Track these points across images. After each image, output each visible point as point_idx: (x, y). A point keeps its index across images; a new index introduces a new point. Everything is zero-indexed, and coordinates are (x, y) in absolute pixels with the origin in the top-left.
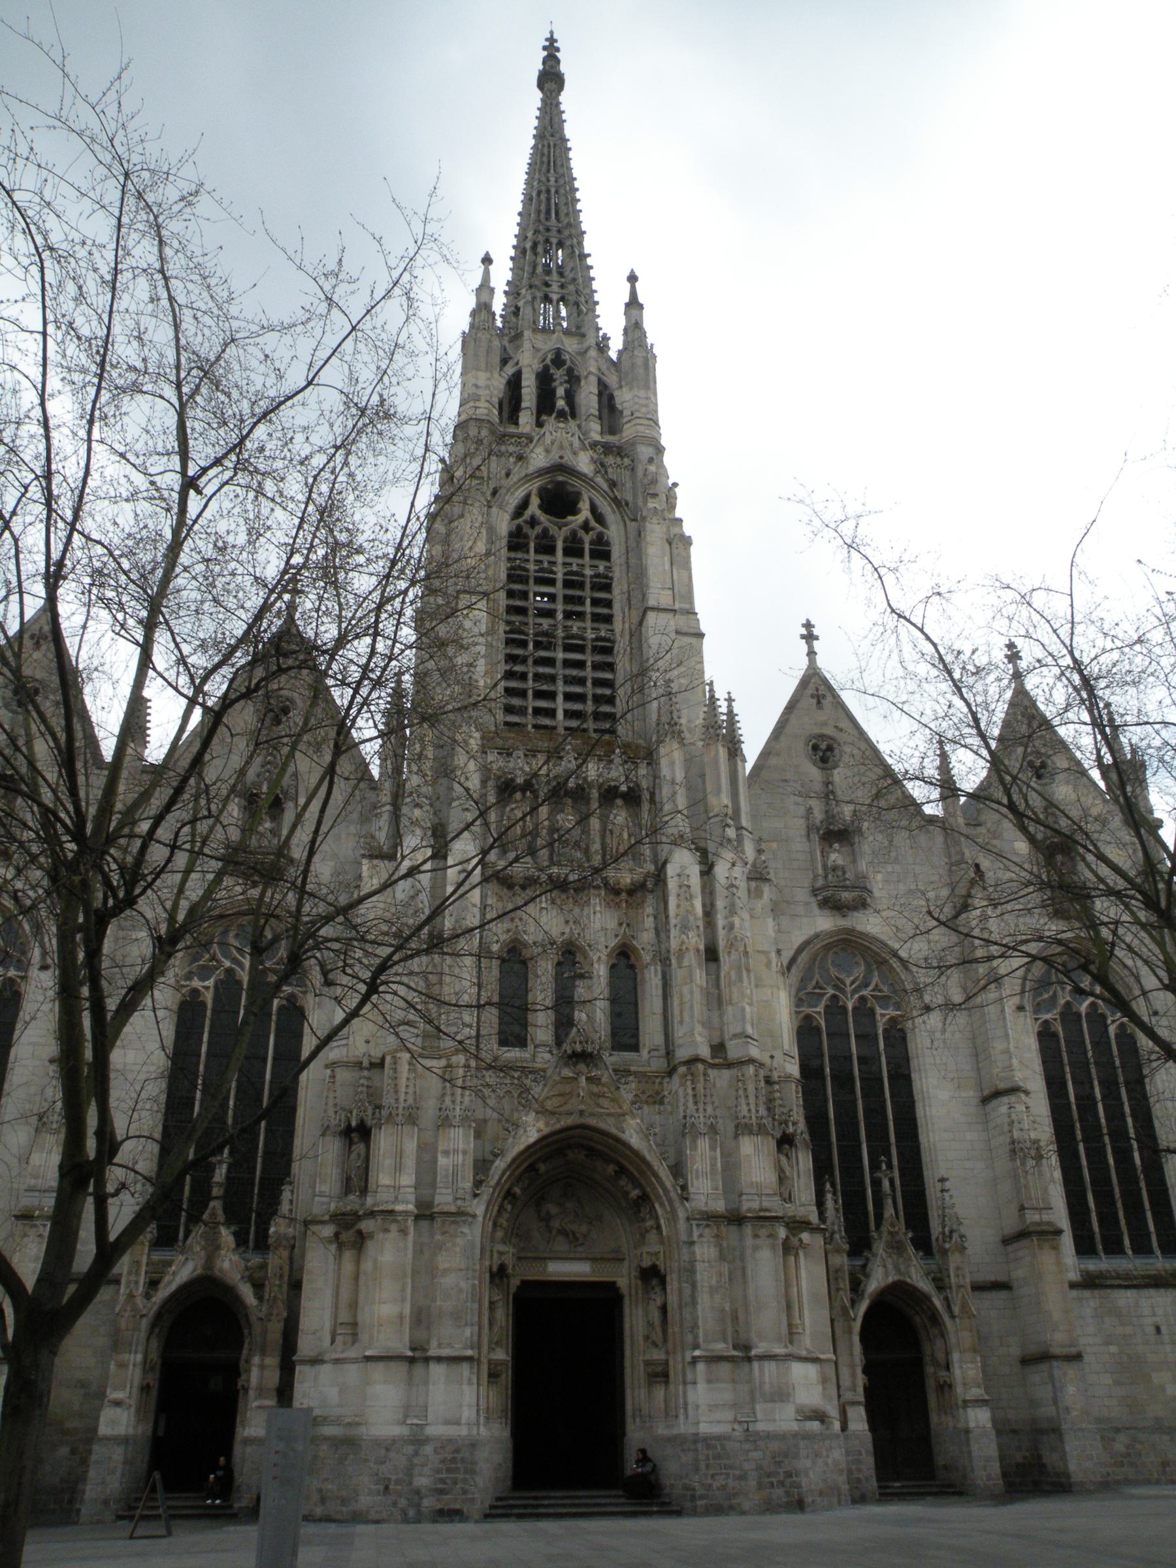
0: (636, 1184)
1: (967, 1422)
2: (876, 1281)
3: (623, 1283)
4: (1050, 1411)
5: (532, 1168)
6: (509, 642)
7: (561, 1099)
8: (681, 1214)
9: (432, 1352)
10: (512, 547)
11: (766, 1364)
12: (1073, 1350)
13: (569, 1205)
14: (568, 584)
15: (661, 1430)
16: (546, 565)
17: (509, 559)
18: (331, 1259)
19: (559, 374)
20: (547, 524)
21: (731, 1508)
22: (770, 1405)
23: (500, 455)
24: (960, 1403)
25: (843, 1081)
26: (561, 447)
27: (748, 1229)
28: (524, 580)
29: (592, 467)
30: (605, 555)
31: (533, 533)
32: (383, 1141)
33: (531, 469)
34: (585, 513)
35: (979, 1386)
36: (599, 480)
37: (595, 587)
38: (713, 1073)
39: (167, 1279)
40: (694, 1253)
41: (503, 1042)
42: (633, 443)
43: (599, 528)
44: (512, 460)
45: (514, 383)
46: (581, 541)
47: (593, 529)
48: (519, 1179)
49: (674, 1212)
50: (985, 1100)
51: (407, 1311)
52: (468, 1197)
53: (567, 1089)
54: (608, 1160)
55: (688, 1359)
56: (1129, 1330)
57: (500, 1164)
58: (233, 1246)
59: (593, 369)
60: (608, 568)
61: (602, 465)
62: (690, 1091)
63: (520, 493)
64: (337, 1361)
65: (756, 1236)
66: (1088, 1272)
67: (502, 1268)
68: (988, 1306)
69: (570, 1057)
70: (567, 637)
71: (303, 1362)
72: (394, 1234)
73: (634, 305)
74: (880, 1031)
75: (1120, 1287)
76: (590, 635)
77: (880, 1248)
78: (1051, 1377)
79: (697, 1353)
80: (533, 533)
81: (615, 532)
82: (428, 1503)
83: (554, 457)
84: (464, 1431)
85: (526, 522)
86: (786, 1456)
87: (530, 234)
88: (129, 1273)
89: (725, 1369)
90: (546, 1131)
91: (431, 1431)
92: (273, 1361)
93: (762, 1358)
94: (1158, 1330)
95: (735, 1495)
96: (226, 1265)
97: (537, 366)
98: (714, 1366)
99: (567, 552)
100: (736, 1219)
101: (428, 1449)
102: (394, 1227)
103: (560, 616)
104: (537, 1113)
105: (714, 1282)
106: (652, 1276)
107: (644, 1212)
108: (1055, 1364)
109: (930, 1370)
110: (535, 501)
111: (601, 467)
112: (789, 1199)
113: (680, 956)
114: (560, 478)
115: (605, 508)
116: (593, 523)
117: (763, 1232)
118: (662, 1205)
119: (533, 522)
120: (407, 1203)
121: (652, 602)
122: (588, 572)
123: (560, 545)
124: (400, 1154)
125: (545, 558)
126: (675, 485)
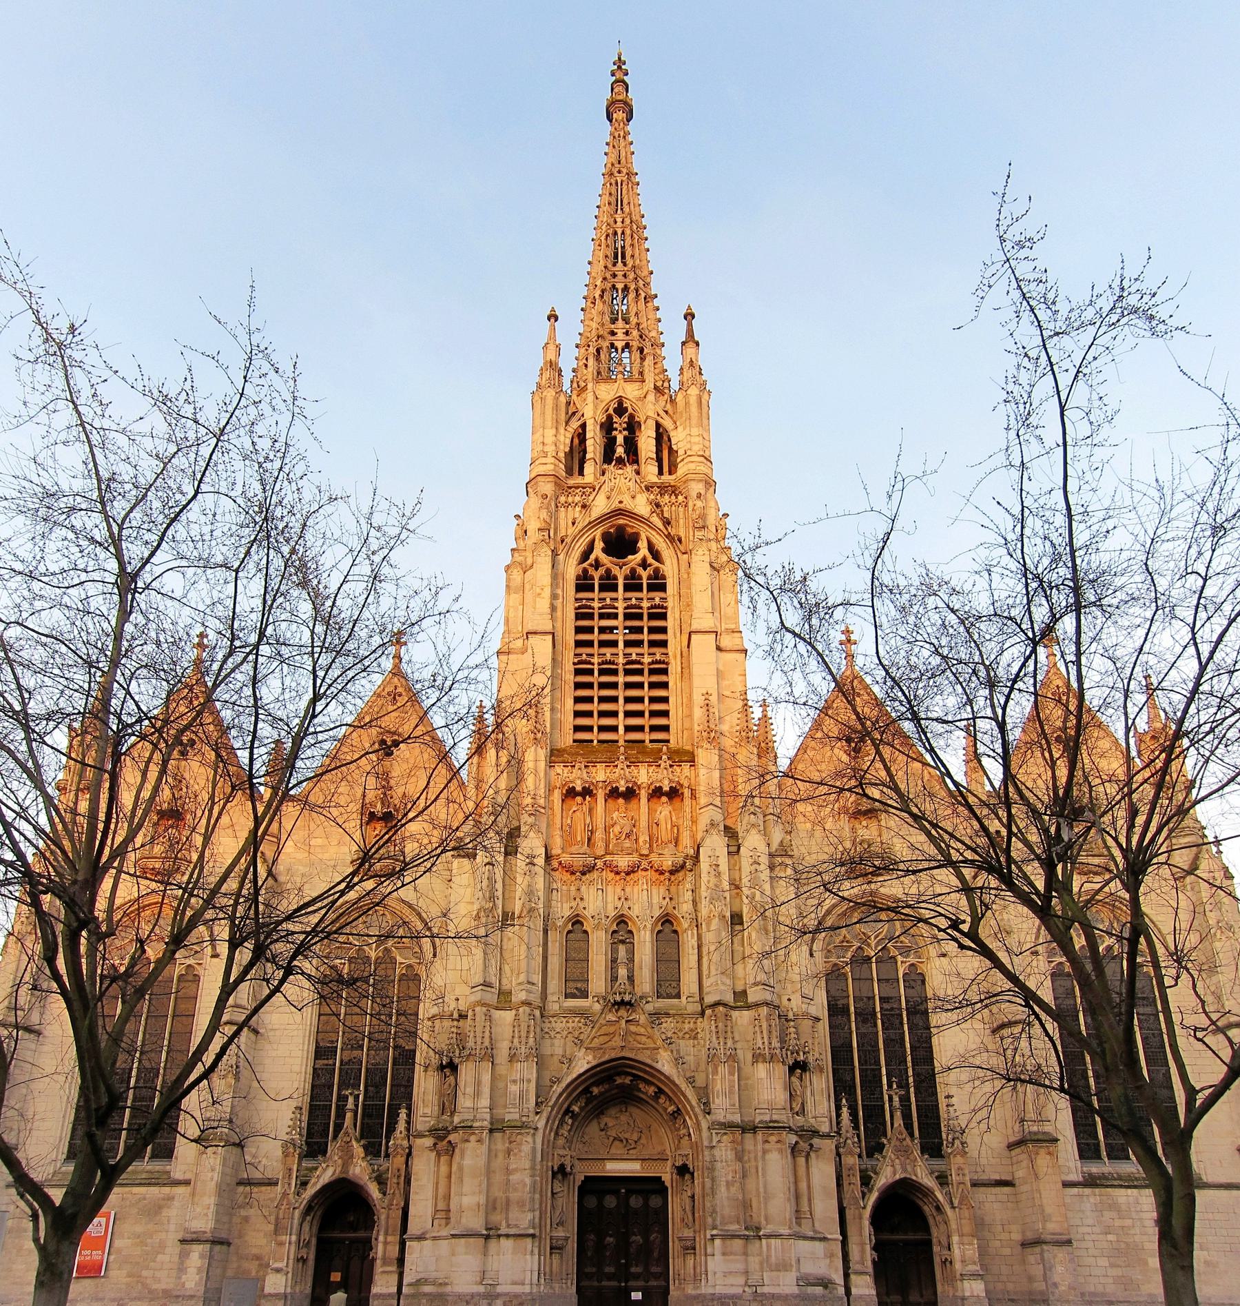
1: (963, 1290)
2: (885, 1177)
3: (666, 1178)
4: (1041, 1286)
5: (587, 1090)
6: (578, 672)
8: (704, 1125)
9: (503, 1231)
10: (579, 588)
12: (1065, 1237)
14: (628, 617)
15: (690, 1290)
16: (608, 601)
20: (609, 565)
22: (775, 1273)
23: (567, 505)
24: (958, 1276)
25: (866, 1016)
26: (620, 492)
27: (760, 1136)
29: (649, 508)
30: (662, 588)
31: (597, 575)
32: (466, 1072)
34: (643, 551)
35: (974, 1263)
38: (735, 1014)
39: (313, 1180)
43: (656, 564)
46: (640, 578)
48: (576, 1099)
49: (698, 1124)
50: (994, 1031)
53: (612, 1029)
55: (708, 1237)
56: (1128, 1222)
57: (558, 1089)
58: (363, 1155)
61: (658, 505)
62: (713, 1028)
64: (435, 1238)
65: (767, 1141)
66: (1090, 1174)
67: (562, 1167)
68: (992, 1202)
69: (613, 1005)
70: (628, 663)
71: (411, 1239)
73: (690, 339)
74: (901, 975)
75: (1121, 1186)
76: (647, 659)
77: (889, 1152)
78: (1043, 1259)
79: (715, 1232)
80: (597, 575)
81: (669, 568)
83: (615, 505)
84: (527, 1289)
85: (591, 565)
87: (598, 283)
89: (738, 1244)
90: (594, 1063)
92: (394, 1239)
93: (769, 1236)
96: (357, 1170)
97: (602, 418)
98: (728, 1242)
99: (627, 588)
100: (748, 1128)
102: (473, 1138)
104: (587, 1049)
105: (730, 1178)
107: (679, 1121)
108: (1045, 1247)
109: (936, 1249)
110: (599, 545)
112: (802, 1111)
114: (621, 522)
115: (661, 544)
116: (650, 560)
117: (773, 1139)
119: (597, 564)
121: (695, 627)
122: (645, 604)
123: (621, 582)
124: (478, 1083)
125: (608, 595)
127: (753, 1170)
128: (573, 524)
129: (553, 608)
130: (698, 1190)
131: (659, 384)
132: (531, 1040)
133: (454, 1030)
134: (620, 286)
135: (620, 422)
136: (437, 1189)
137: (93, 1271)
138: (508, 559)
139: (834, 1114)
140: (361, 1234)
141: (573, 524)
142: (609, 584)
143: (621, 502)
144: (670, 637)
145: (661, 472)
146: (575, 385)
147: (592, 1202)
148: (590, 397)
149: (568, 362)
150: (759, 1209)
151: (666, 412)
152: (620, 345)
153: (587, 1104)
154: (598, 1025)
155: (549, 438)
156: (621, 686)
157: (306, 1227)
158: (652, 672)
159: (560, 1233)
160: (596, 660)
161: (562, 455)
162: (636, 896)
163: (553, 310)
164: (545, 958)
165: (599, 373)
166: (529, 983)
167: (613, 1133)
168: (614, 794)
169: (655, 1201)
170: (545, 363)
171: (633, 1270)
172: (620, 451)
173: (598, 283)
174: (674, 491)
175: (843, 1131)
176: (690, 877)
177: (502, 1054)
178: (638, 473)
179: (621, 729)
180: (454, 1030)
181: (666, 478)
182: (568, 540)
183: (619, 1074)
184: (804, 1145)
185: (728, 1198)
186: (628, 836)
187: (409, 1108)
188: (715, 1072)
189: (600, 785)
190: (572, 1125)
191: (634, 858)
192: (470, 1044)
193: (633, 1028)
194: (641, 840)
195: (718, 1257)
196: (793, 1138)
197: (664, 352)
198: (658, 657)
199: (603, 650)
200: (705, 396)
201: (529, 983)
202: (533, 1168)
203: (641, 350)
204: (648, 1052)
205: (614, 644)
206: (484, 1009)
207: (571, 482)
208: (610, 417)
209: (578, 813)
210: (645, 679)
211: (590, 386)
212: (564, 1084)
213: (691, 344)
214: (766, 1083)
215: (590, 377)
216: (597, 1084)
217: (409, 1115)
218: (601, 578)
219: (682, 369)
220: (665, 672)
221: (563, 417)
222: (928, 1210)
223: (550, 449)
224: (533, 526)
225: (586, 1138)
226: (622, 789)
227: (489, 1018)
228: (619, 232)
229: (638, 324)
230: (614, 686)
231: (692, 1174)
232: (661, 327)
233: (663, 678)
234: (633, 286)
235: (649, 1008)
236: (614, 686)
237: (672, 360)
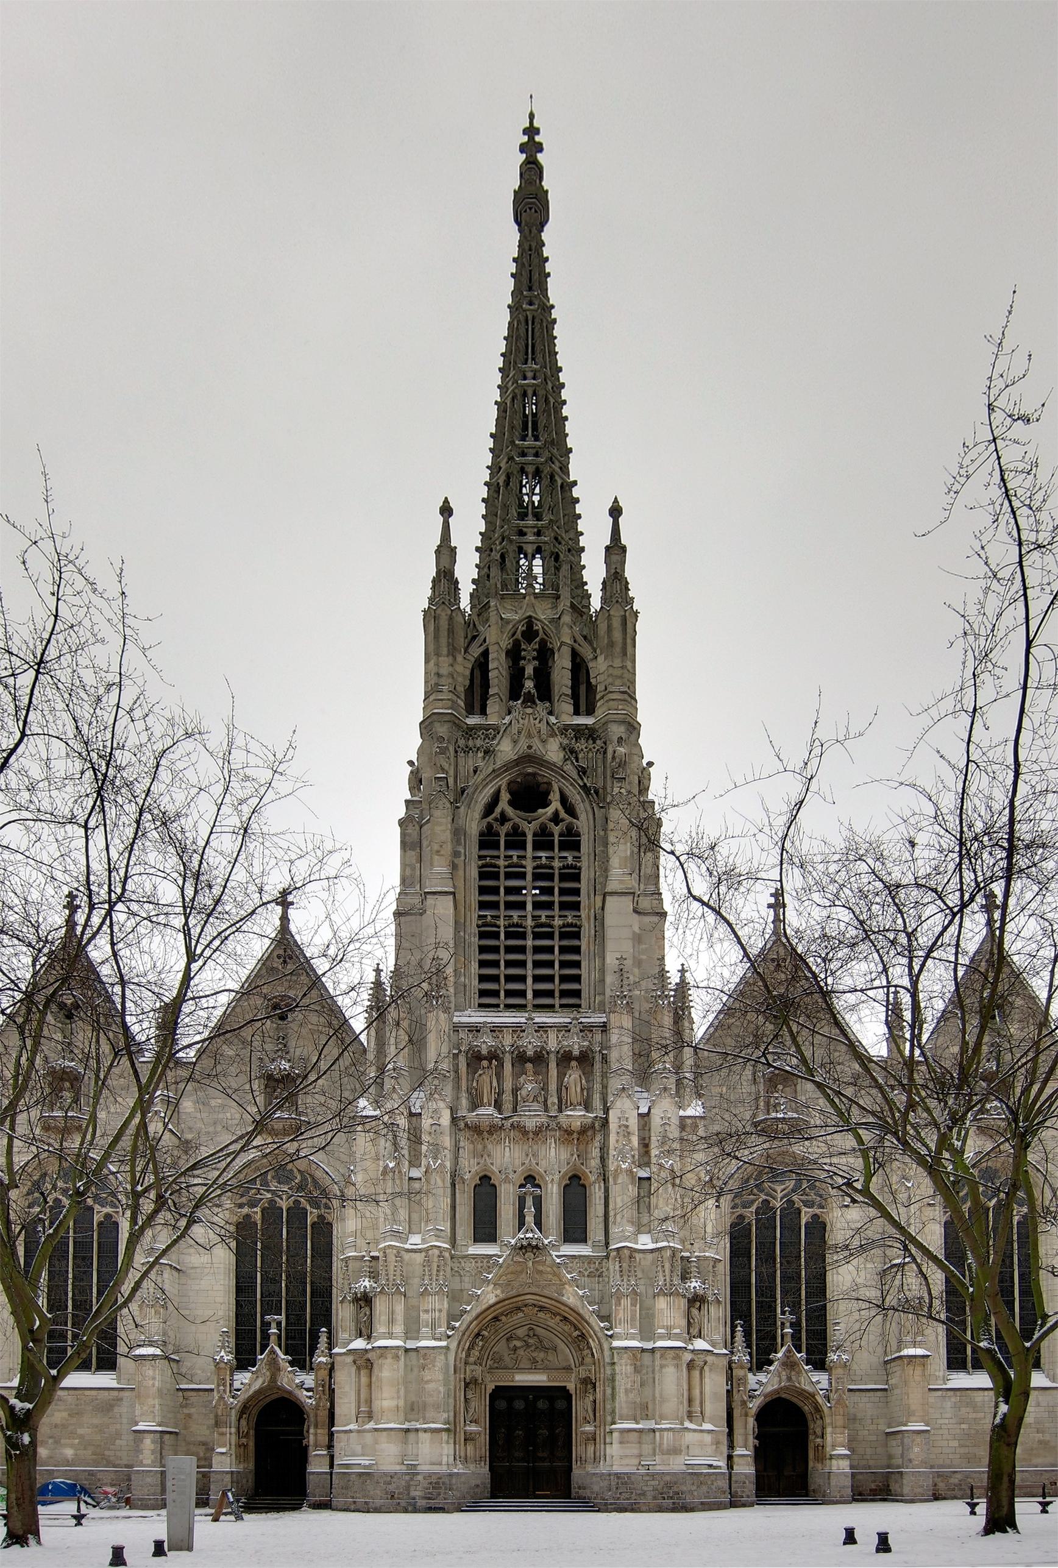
3: (571, 1387)
10: (482, 845)
13: (531, 1341)
15: (590, 1469)
16: (515, 859)
17: (480, 857)
18: (353, 1375)
19: (529, 650)
20: (517, 820)
23: (467, 750)
24: (828, 1456)
28: (495, 876)
29: (561, 755)
30: (575, 846)
31: (503, 830)
33: (499, 764)
34: (555, 805)
37: (563, 878)
40: (614, 1370)
45: (482, 665)
47: (563, 820)
51: (401, 1403)
59: (568, 640)
60: (577, 858)
61: (572, 751)
63: (489, 791)
70: (537, 926)
71: (612, 894)
72: (389, 1361)
73: (616, 550)
81: (583, 824)
84: (445, 1468)
85: (496, 819)
90: (502, 1296)
94: (412, 1370)
97: (506, 643)
99: (537, 846)
101: (420, 1478)
103: (529, 907)
105: (629, 1386)
106: (589, 1384)
109: (811, 1437)
110: (505, 797)
111: (571, 752)
113: (615, 1178)
114: (530, 770)
115: (576, 797)
116: (563, 814)
119: (503, 819)
122: (557, 864)
125: (514, 853)
126: (650, 764)
127: (651, 1380)
128: (475, 772)
130: (599, 1396)
135: (529, 650)
136: (359, 1394)
139: (729, 1337)
141: (475, 772)
147: (502, 1405)
150: (654, 1410)
151: (585, 637)
158: (563, 935)
162: (543, 1152)
169: (560, 1405)
171: (540, 1455)
172: (529, 685)
174: (590, 734)
185: (626, 1402)
190: (483, 1347)
194: (549, 1102)
198: (570, 920)
206: (395, 1251)
214: (666, 1313)
218: (507, 835)
220: (577, 936)
221: (461, 642)
231: (594, 1385)
237: (594, 573)
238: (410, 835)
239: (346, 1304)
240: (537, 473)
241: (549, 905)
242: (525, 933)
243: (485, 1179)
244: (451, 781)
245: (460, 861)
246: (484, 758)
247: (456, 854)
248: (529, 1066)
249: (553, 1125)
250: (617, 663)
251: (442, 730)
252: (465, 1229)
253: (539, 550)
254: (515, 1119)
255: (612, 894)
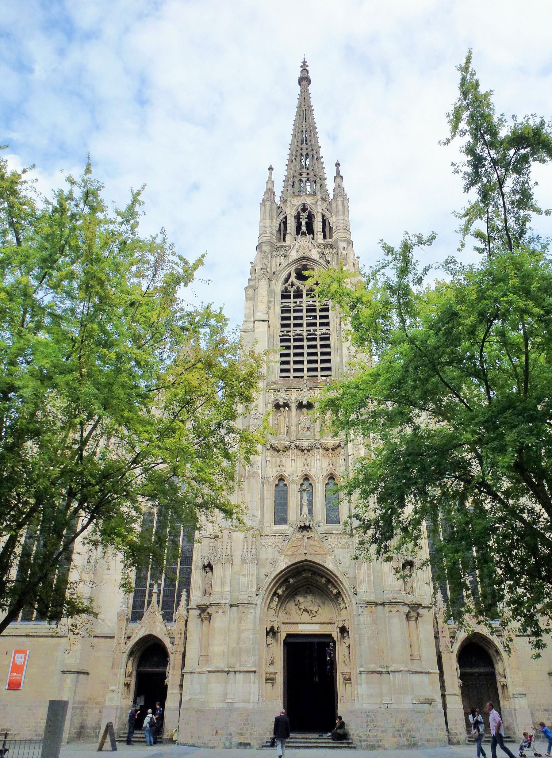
0: (335, 587)
5: (286, 581)
7: (294, 549)
8: (354, 602)
10: (283, 297)
11: (396, 675)
14: (308, 311)
20: (299, 285)
21: (379, 746)
23: (276, 256)
26: (304, 249)
28: (314, 310)
29: (318, 256)
31: (292, 290)
33: (290, 261)
36: (321, 261)
41: (276, 523)
42: (337, 241)
44: (282, 258)
52: (254, 595)
53: (299, 543)
54: (323, 576)
58: (162, 620)
59: (320, 210)
61: (323, 254)
65: (390, 611)
67: (272, 628)
69: (300, 528)
70: (309, 335)
71: (187, 673)
73: (338, 176)
76: (318, 333)
79: (362, 669)
80: (292, 290)
82: (236, 740)
83: (301, 255)
84: (251, 706)
85: (289, 285)
86: (407, 721)
87: (294, 153)
88: (118, 634)
91: (235, 706)
95: (381, 740)
97: (294, 213)
101: (235, 714)
102: (220, 611)
105: (370, 634)
107: (340, 600)
109: (498, 677)
110: (293, 275)
112: (411, 593)
114: (304, 263)
117: (394, 610)
118: (346, 596)
119: (292, 285)
120: (226, 599)
123: (305, 293)
124: (224, 577)
125: (298, 300)
128: (280, 265)
129: (269, 308)
131: (324, 197)
132: (254, 550)
133: (212, 544)
134: (304, 154)
135: (304, 215)
136: (201, 641)
137: (308, 532)
138: (247, 284)
140: (160, 669)
141: (280, 265)
142: (298, 295)
143: (304, 253)
144: (330, 320)
145: (325, 238)
146: (282, 199)
148: (289, 204)
149: (278, 189)
151: (328, 210)
152: (304, 180)
153: (287, 589)
154: (291, 541)
155: (268, 224)
156: (305, 347)
157: (130, 663)
158: (322, 339)
159: (272, 669)
160: (291, 334)
161: (274, 232)
162: (313, 464)
163: (271, 166)
164: (262, 500)
165: (294, 193)
166: (253, 516)
167: (302, 607)
168: (301, 406)
170: (267, 190)
172: (304, 229)
173: (294, 153)
174: (331, 246)
175: (438, 603)
176: (343, 452)
177: (237, 559)
178: (313, 239)
179: (305, 370)
180: (212, 544)
181: (328, 241)
182: (277, 273)
183: (304, 570)
184: (412, 614)
186: (308, 429)
187: (188, 592)
188: (359, 569)
189: (293, 401)
190: (279, 601)
191: (312, 442)
192: (220, 553)
193: (311, 542)
194: (315, 431)
195: (364, 685)
196: (407, 609)
197: (327, 182)
198: (324, 331)
199: (295, 329)
200: (346, 202)
201: (253, 516)
202: (254, 629)
203: (315, 182)
204: (321, 557)
205: (301, 325)
207: (279, 245)
208: (299, 213)
209: (281, 417)
210: (318, 343)
211: (288, 199)
212: (272, 577)
213: (339, 178)
215: (289, 195)
216: (292, 577)
217: (188, 596)
218: (294, 292)
219: (334, 189)
220: (328, 339)
221: (275, 214)
222: (492, 652)
223: (268, 230)
224: (258, 267)
225: (287, 609)
226: (305, 403)
227: (230, 537)
228: (304, 131)
229: (313, 170)
230: (301, 347)
231: (348, 632)
232: (325, 171)
233: (327, 342)
234: (310, 154)
235: (321, 530)
236: (301, 347)
237: (330, 186)
238: (249, 294)
239: (198, 571)
240: (307, 155)
241: (314, 324)
242: (303, 339)
243: (281, 479)
244: (269, 269)
245: (271, 305)
246: (378, 559)
247: (270, 302)
248: (304, 409)
249: (318, 445)
250: (341, 217)
251: (266, 248)
252: (269, 516)
253: (308, 180)
254: (297, 442)
255: (187, 673)
